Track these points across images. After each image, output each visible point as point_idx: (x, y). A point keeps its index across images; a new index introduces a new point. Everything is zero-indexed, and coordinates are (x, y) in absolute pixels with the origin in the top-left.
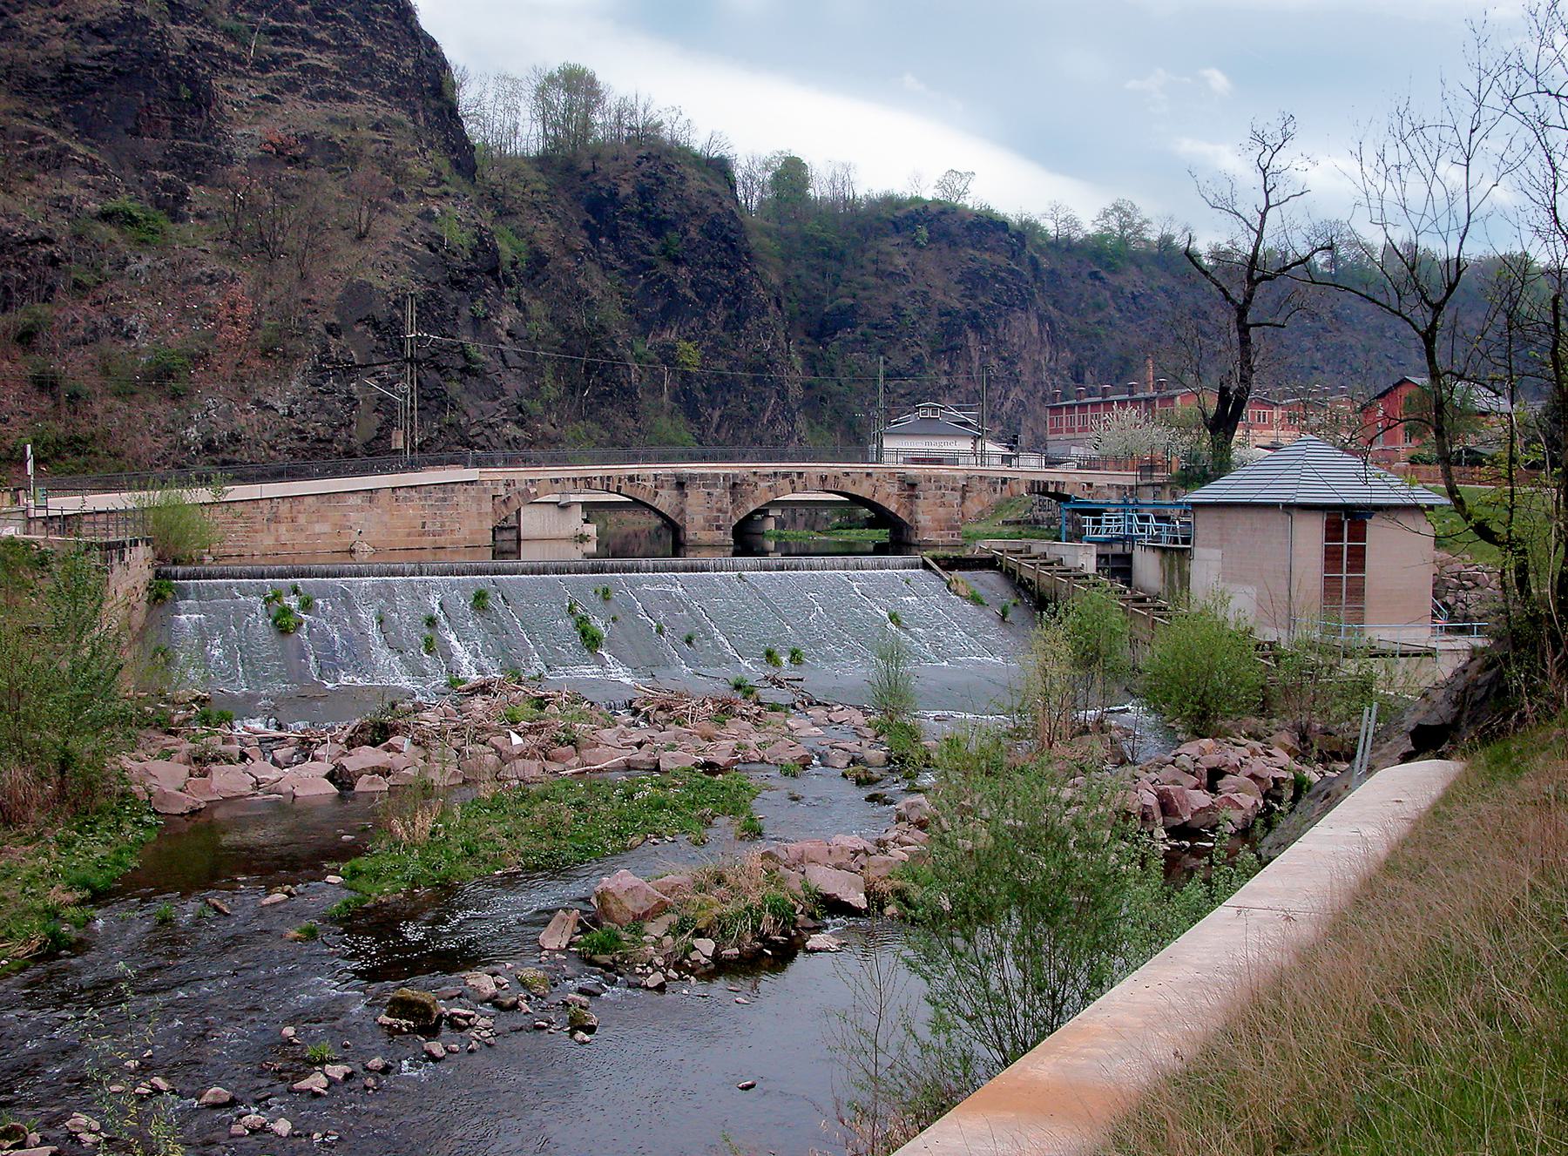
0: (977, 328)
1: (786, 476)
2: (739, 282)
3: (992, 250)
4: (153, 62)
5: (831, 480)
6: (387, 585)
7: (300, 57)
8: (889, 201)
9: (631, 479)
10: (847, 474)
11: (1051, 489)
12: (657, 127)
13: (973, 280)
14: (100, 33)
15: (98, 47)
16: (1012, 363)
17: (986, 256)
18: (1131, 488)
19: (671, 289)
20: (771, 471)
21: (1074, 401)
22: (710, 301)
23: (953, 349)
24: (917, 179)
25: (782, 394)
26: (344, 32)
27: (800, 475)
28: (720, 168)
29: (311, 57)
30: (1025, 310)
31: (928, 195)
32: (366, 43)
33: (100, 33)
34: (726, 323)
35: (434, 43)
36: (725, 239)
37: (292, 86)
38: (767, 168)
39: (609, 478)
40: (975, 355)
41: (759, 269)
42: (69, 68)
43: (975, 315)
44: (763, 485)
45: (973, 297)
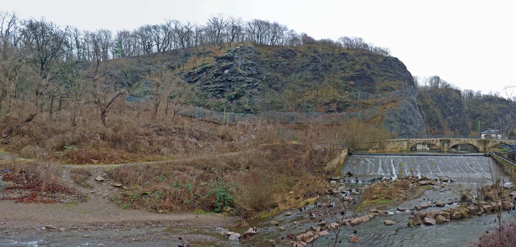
0: (501, 117)
1: (458, 140)
2: (461, 109)
3: (503, 104)
4: (365, 75)
5: (465, 141)
6: (390, 157)
7: (388, 75)
8: (487, 96)
9: (432, 140)
11: (503, 143)
12: (488, 95)
13: (500, 109)
14: (357, 71)
15: (357, 73)
16: (507, 122)
17: (502, 105)
19: (450, 111)
20: (455, 139)
22: (456, 113)
23: (496, 120)
24: (491, 91)
25: (467, 127)
26: (395, 71)
27: (460, 140)
28: (458, 92)
29: (390, 74)
30: (509, 114)
31: (493, 95)
32: (398, 72)
33: (357, 71)
34: (459, 116)
35: (410, 72)
36: (459, 103)
37: (386, 79)
38: (390, 55)
40: (500, 121)
41: (464, 108)
42: (353, 76)
43: (500, 114)
44: (454, 142)
45: (500, 112)
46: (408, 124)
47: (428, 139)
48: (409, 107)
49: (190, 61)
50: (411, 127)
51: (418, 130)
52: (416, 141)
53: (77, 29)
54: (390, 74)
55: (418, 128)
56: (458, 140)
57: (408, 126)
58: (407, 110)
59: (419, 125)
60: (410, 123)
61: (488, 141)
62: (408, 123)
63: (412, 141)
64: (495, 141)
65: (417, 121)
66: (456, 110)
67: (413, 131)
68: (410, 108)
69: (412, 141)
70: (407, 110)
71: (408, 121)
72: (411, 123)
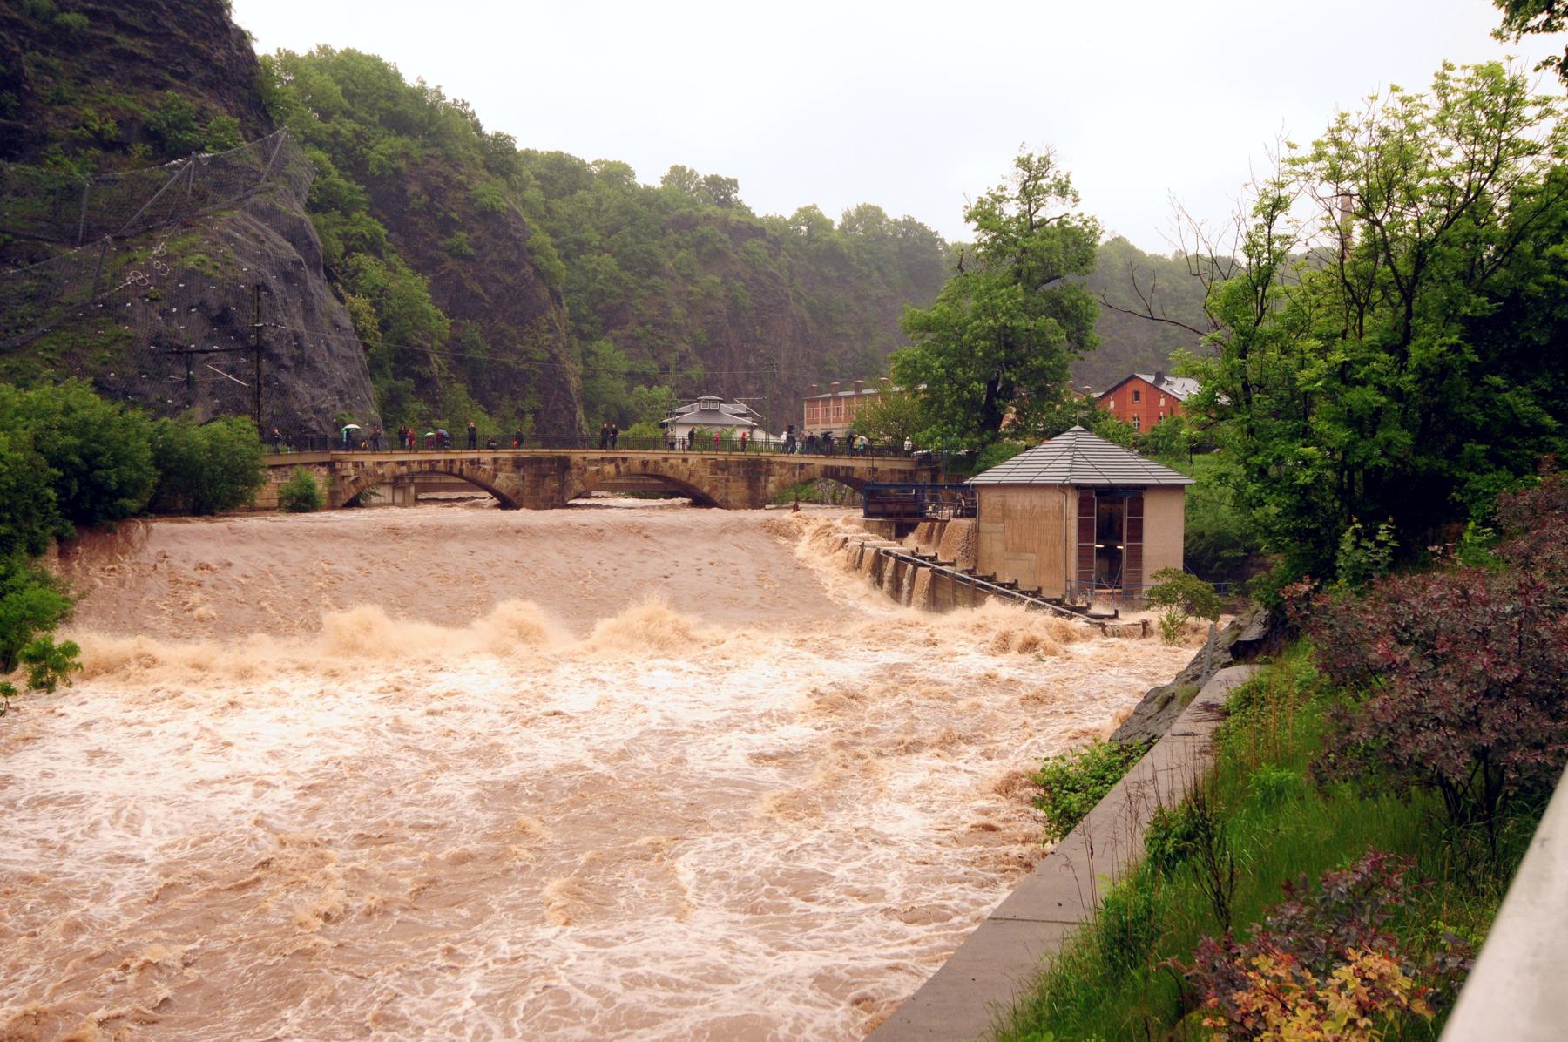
1: (612, 461)
9: (472, 462)
10: (666, 460)
18: (911, 472)
21: (829, 395)
27: (624, 460)
29: (123, 41)
39: (452, 461)
46: (287, 368)
47: (449, 457)
48: (281, 263)
49: (1411, 225)
50: (300, 386)
51: (342, 400)
52: (379, 464)
53: (1315, 139)
54: (123, 41)
55: (340, 393)
56: (612, 461)
57: (285, 377)
58: (272, 280)
59: (340, 373)
60: (292, 358)
61: (769, 463)
62: (287, 362)
63: (356, 464)
64: (802, 466)
65: (329, 349)
66: (497, 281)
67: (318, 411)
68: (290, 268)
69: (356, 464)
70: (272, 280)
71: (282, 350)
72: (303, 363)
